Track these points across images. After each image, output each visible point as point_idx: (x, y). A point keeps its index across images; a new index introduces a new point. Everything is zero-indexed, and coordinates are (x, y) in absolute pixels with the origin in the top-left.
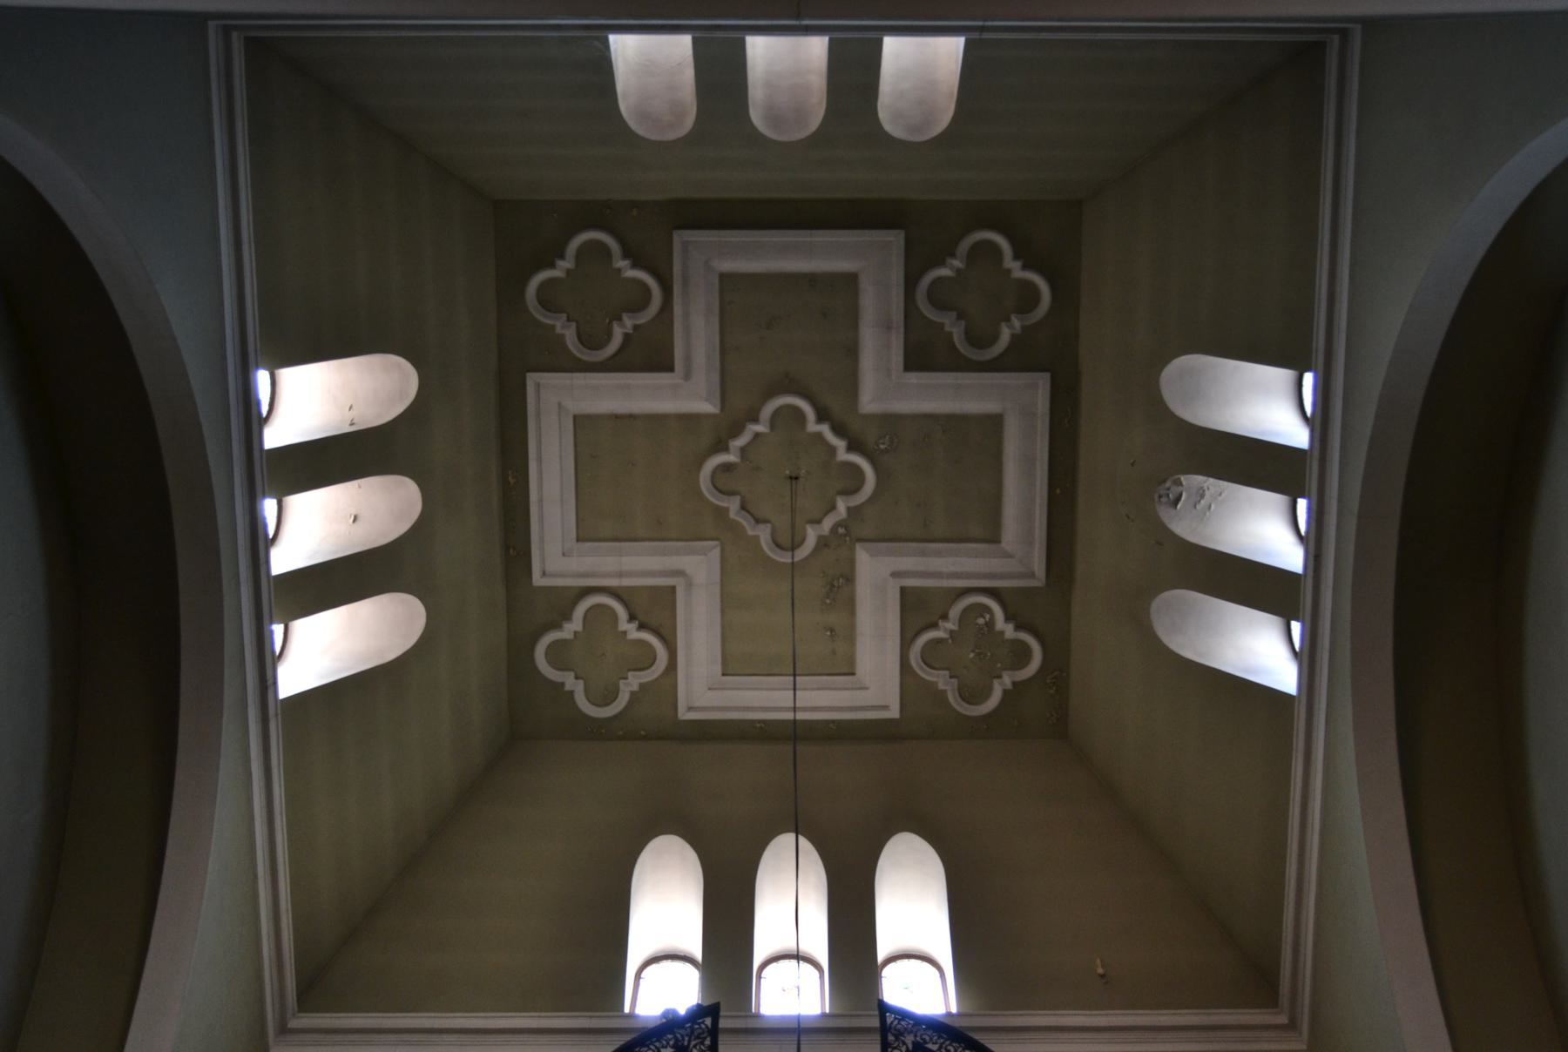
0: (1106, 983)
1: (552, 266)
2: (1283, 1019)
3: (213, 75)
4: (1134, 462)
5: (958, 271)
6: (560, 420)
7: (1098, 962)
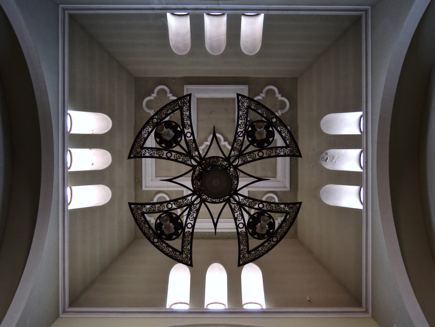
0: (311, 302)
1: (150, 95)
2: (364, 310)
3: (60, 21)
4: (314, 150)
5: (263, 97)
6: (151, 140)
7: (308, 297)
